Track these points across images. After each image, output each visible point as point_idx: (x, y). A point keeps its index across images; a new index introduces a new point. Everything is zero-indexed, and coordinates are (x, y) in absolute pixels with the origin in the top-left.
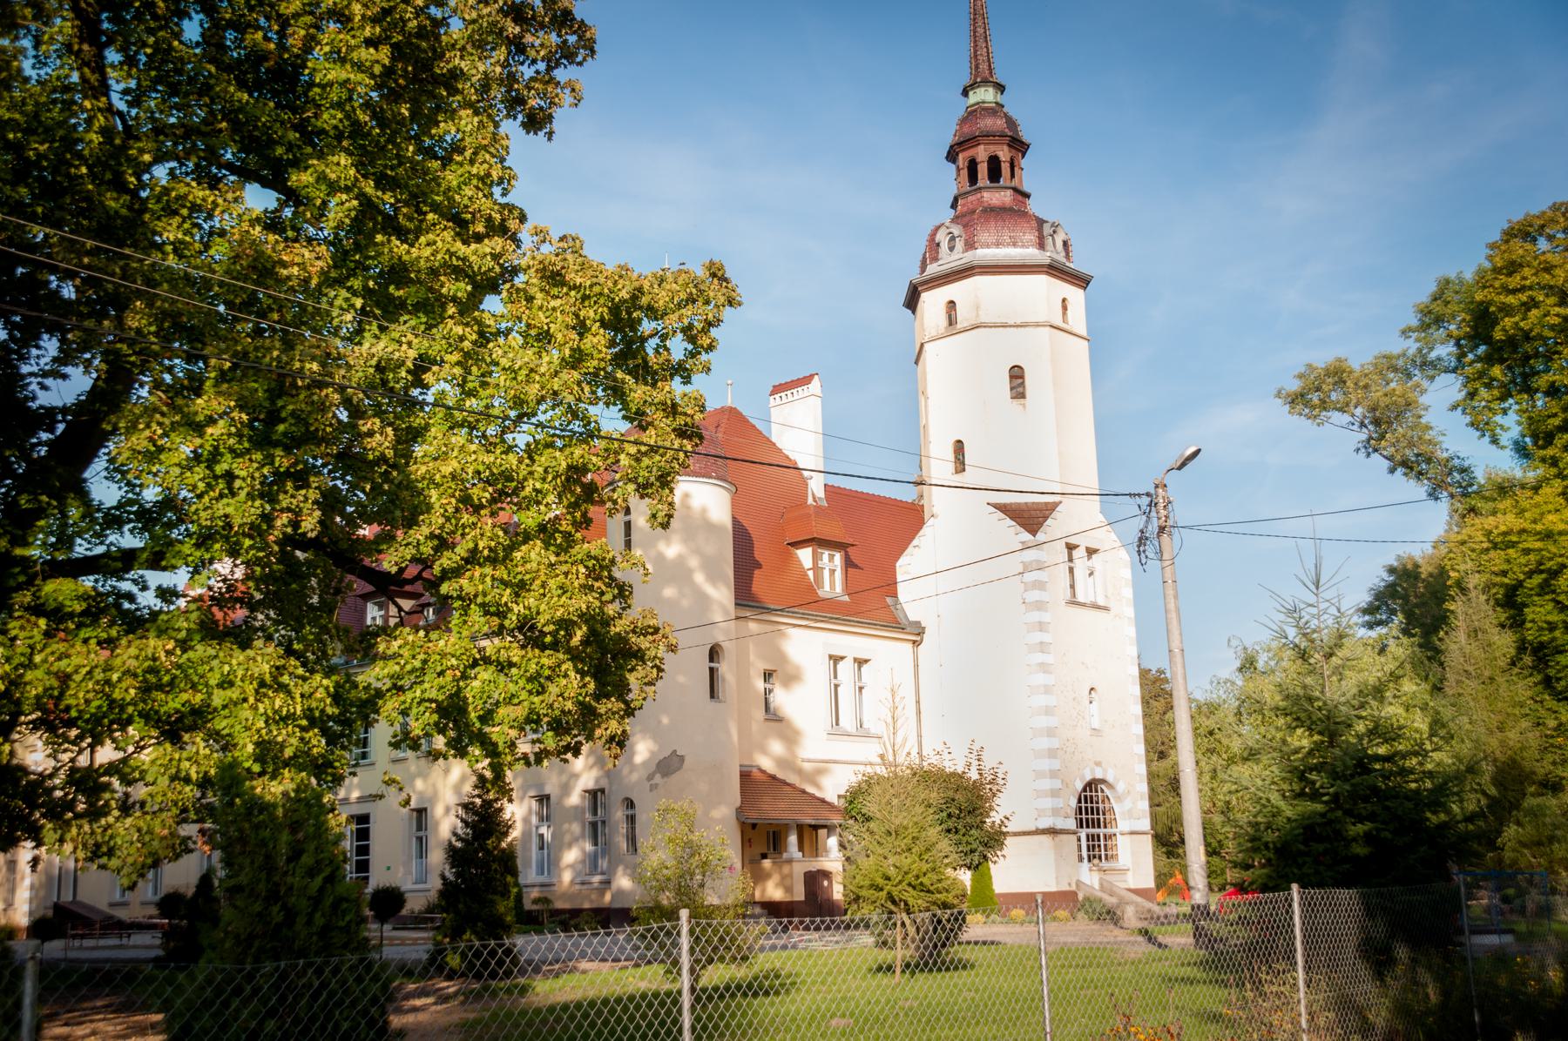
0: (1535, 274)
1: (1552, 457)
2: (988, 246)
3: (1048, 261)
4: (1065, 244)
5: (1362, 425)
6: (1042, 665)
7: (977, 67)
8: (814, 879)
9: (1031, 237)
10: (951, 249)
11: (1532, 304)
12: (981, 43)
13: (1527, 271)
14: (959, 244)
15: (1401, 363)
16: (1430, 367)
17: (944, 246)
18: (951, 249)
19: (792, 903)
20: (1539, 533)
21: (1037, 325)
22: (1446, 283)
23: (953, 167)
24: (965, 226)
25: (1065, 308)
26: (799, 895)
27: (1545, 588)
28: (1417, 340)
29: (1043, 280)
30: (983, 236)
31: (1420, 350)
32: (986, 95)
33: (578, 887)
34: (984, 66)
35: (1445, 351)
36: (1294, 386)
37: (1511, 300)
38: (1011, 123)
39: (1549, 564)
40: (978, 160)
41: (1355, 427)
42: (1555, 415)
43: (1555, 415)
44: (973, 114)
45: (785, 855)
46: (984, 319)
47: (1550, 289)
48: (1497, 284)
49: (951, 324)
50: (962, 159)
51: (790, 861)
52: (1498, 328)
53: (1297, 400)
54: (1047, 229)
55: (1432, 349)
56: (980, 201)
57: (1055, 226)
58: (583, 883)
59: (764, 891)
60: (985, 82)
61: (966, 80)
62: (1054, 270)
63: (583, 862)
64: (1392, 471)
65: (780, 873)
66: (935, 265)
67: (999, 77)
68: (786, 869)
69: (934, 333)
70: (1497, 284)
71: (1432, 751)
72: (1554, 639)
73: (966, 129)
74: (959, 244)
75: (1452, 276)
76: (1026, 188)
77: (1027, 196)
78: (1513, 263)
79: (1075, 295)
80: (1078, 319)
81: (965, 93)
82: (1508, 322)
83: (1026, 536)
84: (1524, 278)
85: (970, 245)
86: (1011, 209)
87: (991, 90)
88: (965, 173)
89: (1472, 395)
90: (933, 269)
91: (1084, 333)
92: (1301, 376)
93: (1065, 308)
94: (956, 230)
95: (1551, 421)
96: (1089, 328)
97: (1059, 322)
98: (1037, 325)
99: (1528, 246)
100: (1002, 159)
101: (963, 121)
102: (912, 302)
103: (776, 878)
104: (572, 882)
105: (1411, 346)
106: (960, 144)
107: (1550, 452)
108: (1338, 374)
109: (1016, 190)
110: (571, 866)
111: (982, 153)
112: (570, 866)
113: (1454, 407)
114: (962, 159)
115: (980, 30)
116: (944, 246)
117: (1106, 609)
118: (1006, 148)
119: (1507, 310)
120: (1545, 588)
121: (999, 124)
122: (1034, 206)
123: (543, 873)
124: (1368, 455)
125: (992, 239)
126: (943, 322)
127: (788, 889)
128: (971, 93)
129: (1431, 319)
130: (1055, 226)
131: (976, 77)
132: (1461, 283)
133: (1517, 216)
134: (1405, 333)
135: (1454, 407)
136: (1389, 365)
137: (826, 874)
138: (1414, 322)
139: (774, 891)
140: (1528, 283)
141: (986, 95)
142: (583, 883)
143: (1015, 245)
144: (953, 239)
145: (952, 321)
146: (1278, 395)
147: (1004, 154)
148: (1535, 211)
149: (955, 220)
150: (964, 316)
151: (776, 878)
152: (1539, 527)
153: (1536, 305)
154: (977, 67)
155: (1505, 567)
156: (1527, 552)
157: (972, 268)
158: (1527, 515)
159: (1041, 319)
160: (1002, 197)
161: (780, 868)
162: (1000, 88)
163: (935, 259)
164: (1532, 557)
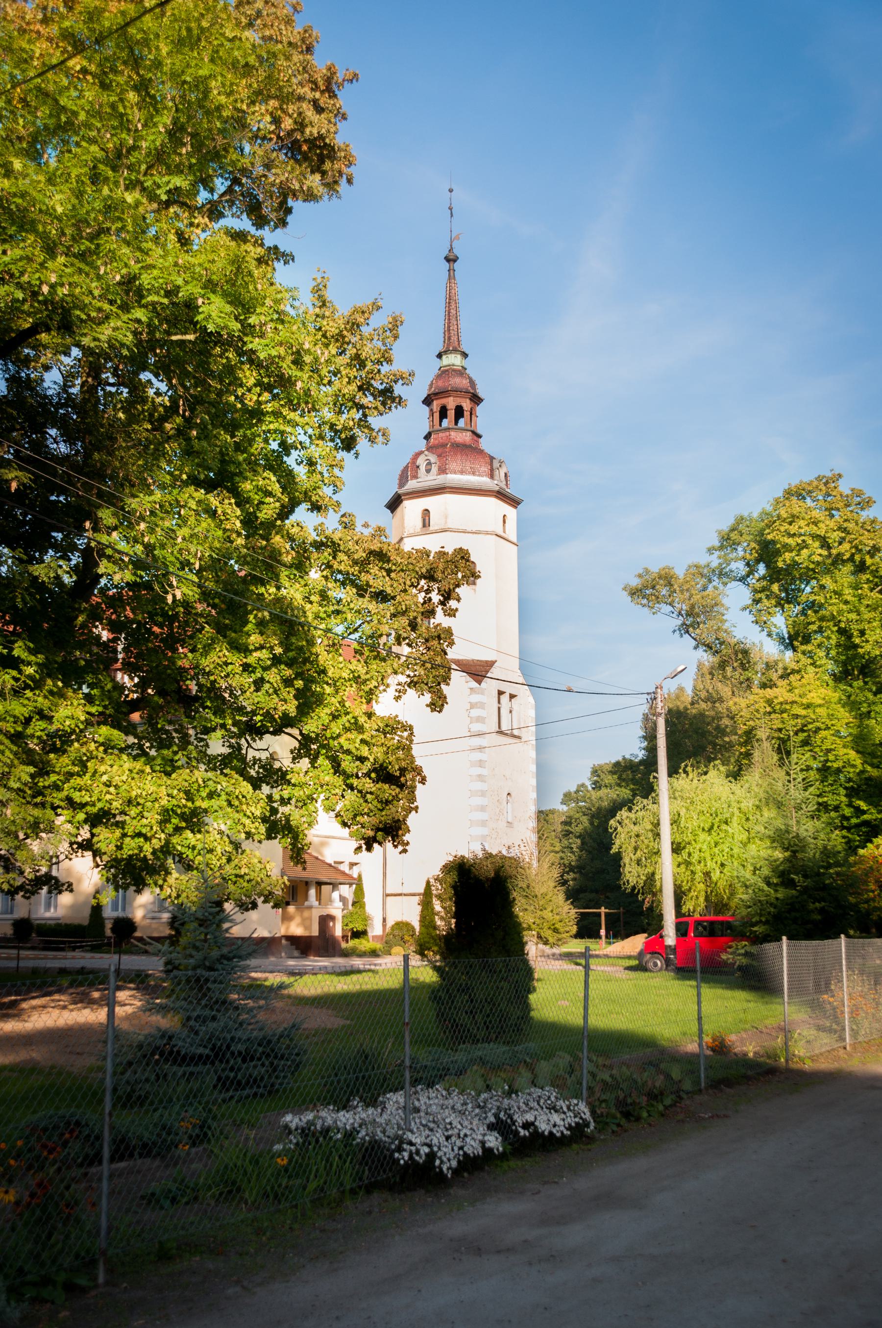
0: (808, 525)
1: (810, 652)
2: (455, 473)
3: (497, 488)
4: (506, 475)
5: (680, 614)
6: (479, 776)
7: (449, 338)
8: (326, 920)
9: (485, 469)
10: (428, 471)
11: (804, 546)
12: (453, 321)
13: (802, 523)
14: (434, 469)
15: (705, 571)
16: (723, 574)
17: (423, 468)
18: (428, 471)
19: (310, 937)
20: (803, 704)
21: (487, 533)
22: (740, 520)
23: (426, 409)
24: (439, 456)
25: (504, 522)
26: (315, 932)
27: (805, 743)
28: (719, 558)
29: (493, 501)
30: (453, 465)
31: (720, 564)
32: (454, 360)
33: (148, 921)
34: (454, 338)
35: (739, 568)
36: (635, 582)
37: (791, 541)
38: (472, 383)
39: (810, 726)
40: (449, 407)
41: (674, 615)
42: (813, 623)
43: (813, 623)
44: (445, 373)
45: (306, 903)
46: (450, 525)
47: (815, 537)
48: (782, 529)
49: (424, 526)
50: (436, 405)
51: (310, 908)
52: (780, 559)
53: (635, 593)
54: (496, 464)
55: (728, 565)
56: (448, 437)
57: (501, 462)
58: (153, 918)
59: (288, 928)
60: (455, 350)
61: (440, 348)
62: (501, 495)
63: (154, 903)
64: (696, 648)
65: (301, 916)
66: (414, 481)
67: (464, 347)
68: (306, 914)
69: (412, 531)
70: (782, 529)
71: (25, 728)
72: (65, 550)
73: (440, 383)
74: (434, 469)
75: (746, 514)
76: (479, 431)
77: (479, 436)
78: (793, 516)
79: (511, 512)
80: (512, 533)
81: (440, 356)
82: (788, 556)
83: (474, 684)
84: (800, 527)
85: (442, 471)
86: (470, 446)
87: (459, 357)
88: (437, 416)
89: (757, 601)
90: (412, 485)
91: (515, 540)
92: (640, 576)
93: (504, 522)
94: (433, 458)
95: (811, 627)
96: (519, 536)
97: (501, 533)
98: (487, 533)
99: (801, 503)
100: (465, 408)
101: (439, 377)
102: (394, 504)
103: (298, 919)
104: (144, 917)
105: (715, 561)
106: (436, 394)
107: (809, 648)
108: (668, 578)
109: (474, 433)
110: (143, 906)
111: (451, 403)
112: (141, 906)
113: (744, 609)
114: (436, 405)
115: (453, 312)
116: (423, 468)
117: (519, 737)
118: (468, 401)
119: (787, 548)
120: (805, 743)
121: (464, 383)
122: (484, 444)
123: (117, 910)
124: (681, 636)
125: (458, 468)
126: (419, 523)
127: (307, 928)
128: (444, 357)
129: (727, 541)
130: (501, 462)
131: (449, 345)
132: (751, 520)
133: (795, 482)
134: (710, 550)
135: (744, 609)
136: (698, 571)
137: (332, 918)
138: (717, 544)
139: (296, 929)
140: (802, 531)
141: (454, 360)
142: (153, 918)
143: (474, 474)
144: (429, 464)
145: (426, 523)
146: (625, 589)
147: (466, 405)
148: (806, 479)
149: (430, 449)
150: (435, 521)
151: (298, 919)
152: (805, 701)
153: (807, 547)
154: (449, 338)
155: (781, 726)
156: (797, 716)
157: (444, 488)
158: (797, 691)
159: (490, 529)
160: (467, 437)
161: (302, 912)
162: (465, 355)
163: (415, 477)
164: (799, 721)
